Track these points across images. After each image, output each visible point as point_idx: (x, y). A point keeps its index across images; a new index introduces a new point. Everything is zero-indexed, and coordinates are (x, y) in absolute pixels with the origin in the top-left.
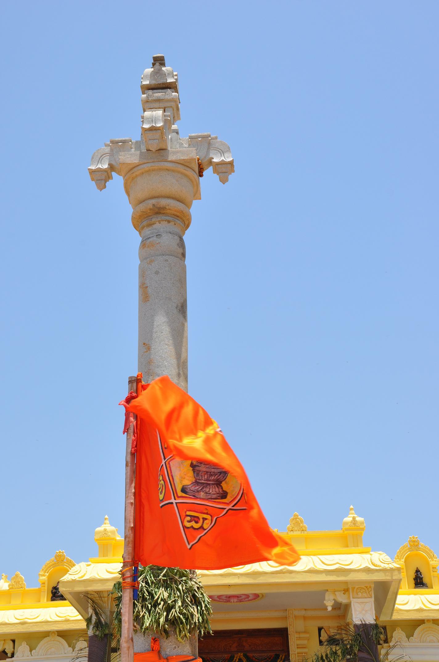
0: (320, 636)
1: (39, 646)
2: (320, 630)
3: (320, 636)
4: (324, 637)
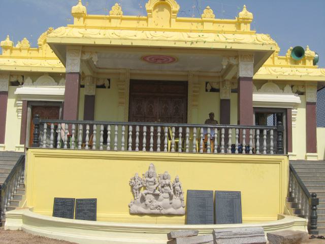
0: (206, 86)
1: (262, 87)
2: (207, 83)
3: (206, 86)
4: (209, 88)
